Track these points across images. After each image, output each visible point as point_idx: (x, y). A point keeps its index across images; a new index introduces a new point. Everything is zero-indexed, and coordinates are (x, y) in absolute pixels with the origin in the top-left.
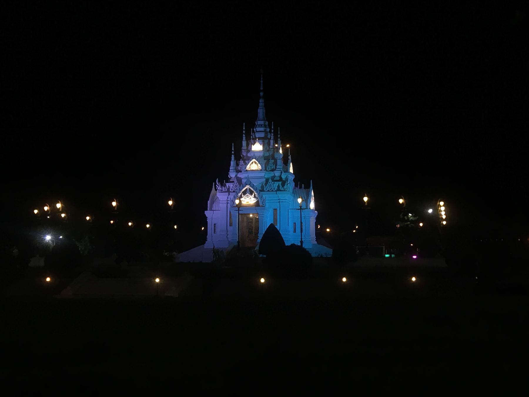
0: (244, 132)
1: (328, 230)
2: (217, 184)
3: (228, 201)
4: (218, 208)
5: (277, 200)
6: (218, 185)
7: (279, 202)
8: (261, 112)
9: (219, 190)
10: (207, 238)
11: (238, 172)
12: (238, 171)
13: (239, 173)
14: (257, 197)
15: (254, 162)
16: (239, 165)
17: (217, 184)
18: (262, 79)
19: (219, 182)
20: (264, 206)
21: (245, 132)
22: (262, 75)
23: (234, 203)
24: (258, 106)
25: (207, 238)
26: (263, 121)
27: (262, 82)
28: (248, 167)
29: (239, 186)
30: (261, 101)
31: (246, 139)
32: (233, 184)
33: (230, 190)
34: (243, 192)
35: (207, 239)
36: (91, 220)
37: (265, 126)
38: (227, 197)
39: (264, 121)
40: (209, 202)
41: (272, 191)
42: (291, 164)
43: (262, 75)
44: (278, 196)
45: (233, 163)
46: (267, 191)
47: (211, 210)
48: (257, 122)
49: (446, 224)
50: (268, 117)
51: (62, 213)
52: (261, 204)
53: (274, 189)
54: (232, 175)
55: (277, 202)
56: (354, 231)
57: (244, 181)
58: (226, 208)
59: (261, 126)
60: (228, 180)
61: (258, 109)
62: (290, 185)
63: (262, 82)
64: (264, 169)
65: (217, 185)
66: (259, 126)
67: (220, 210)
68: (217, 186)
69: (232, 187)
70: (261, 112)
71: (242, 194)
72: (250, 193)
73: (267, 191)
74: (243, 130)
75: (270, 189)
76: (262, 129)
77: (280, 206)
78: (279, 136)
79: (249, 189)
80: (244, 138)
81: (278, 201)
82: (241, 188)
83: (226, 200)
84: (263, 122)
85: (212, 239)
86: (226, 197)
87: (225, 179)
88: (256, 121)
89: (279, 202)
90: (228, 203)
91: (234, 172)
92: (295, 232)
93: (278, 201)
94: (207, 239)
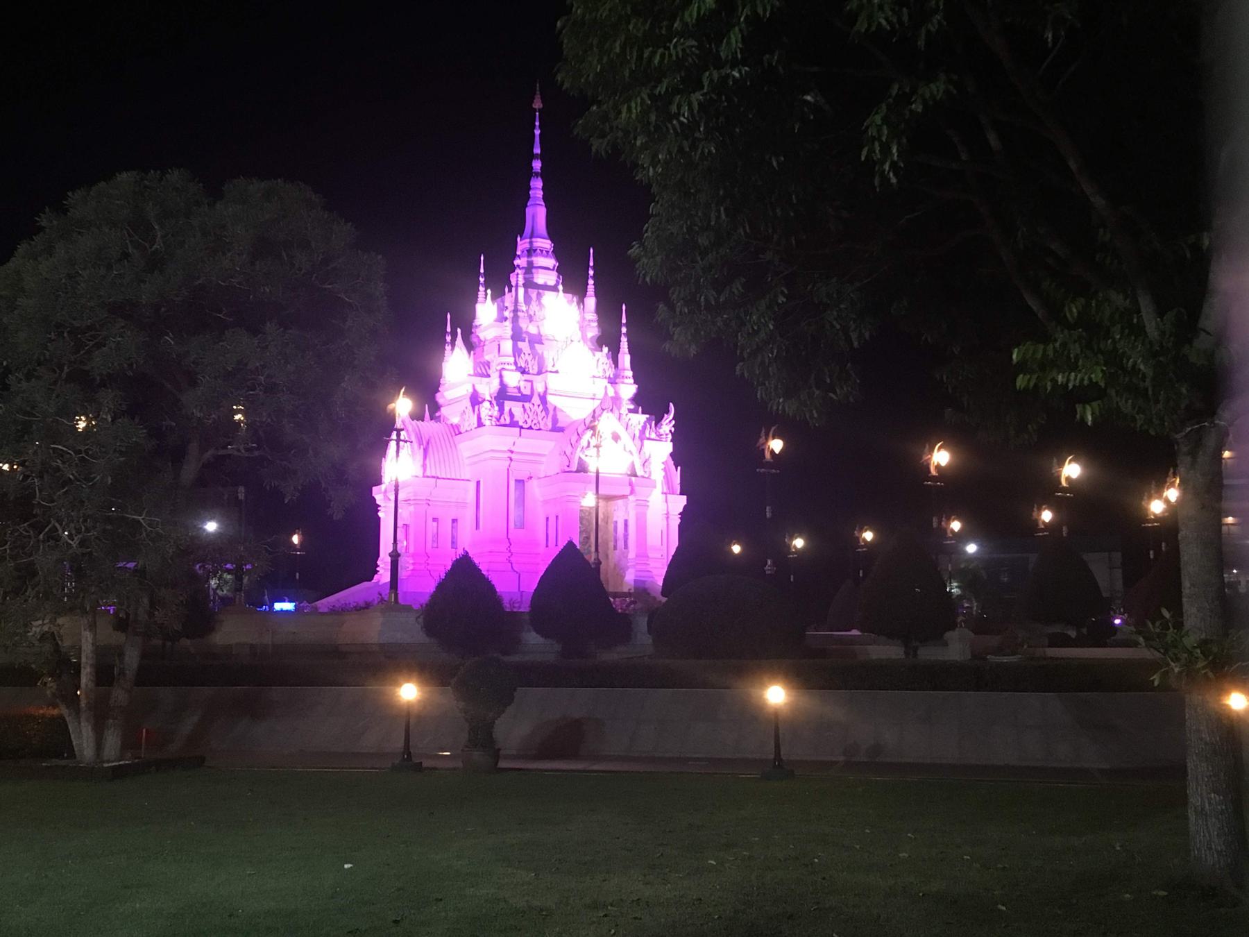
1: (736, 549)
7: (511, 459)
8: (538, 214)
10: (378, 566)
18: (537, 124)
20: (646, 476)
21: (485, 281)
22: (537, 114)
25: (378, 566)
27: (537, 132)
30: (537, 184)
31: (492, 295)
35: (378, 569)
43: (537, 114)
46: (528, 428)
49: (782, 451)
52: (640, 472)
56: (1072, 470)
61: (526, 206)
62: (627, 405)
63: (537, 132)
70: (538, 214)
73: (528, 428)
74: (620, 324)
78: (591, 273)
82: (573, 441)
85: (428, 564)
94: (378, 569)
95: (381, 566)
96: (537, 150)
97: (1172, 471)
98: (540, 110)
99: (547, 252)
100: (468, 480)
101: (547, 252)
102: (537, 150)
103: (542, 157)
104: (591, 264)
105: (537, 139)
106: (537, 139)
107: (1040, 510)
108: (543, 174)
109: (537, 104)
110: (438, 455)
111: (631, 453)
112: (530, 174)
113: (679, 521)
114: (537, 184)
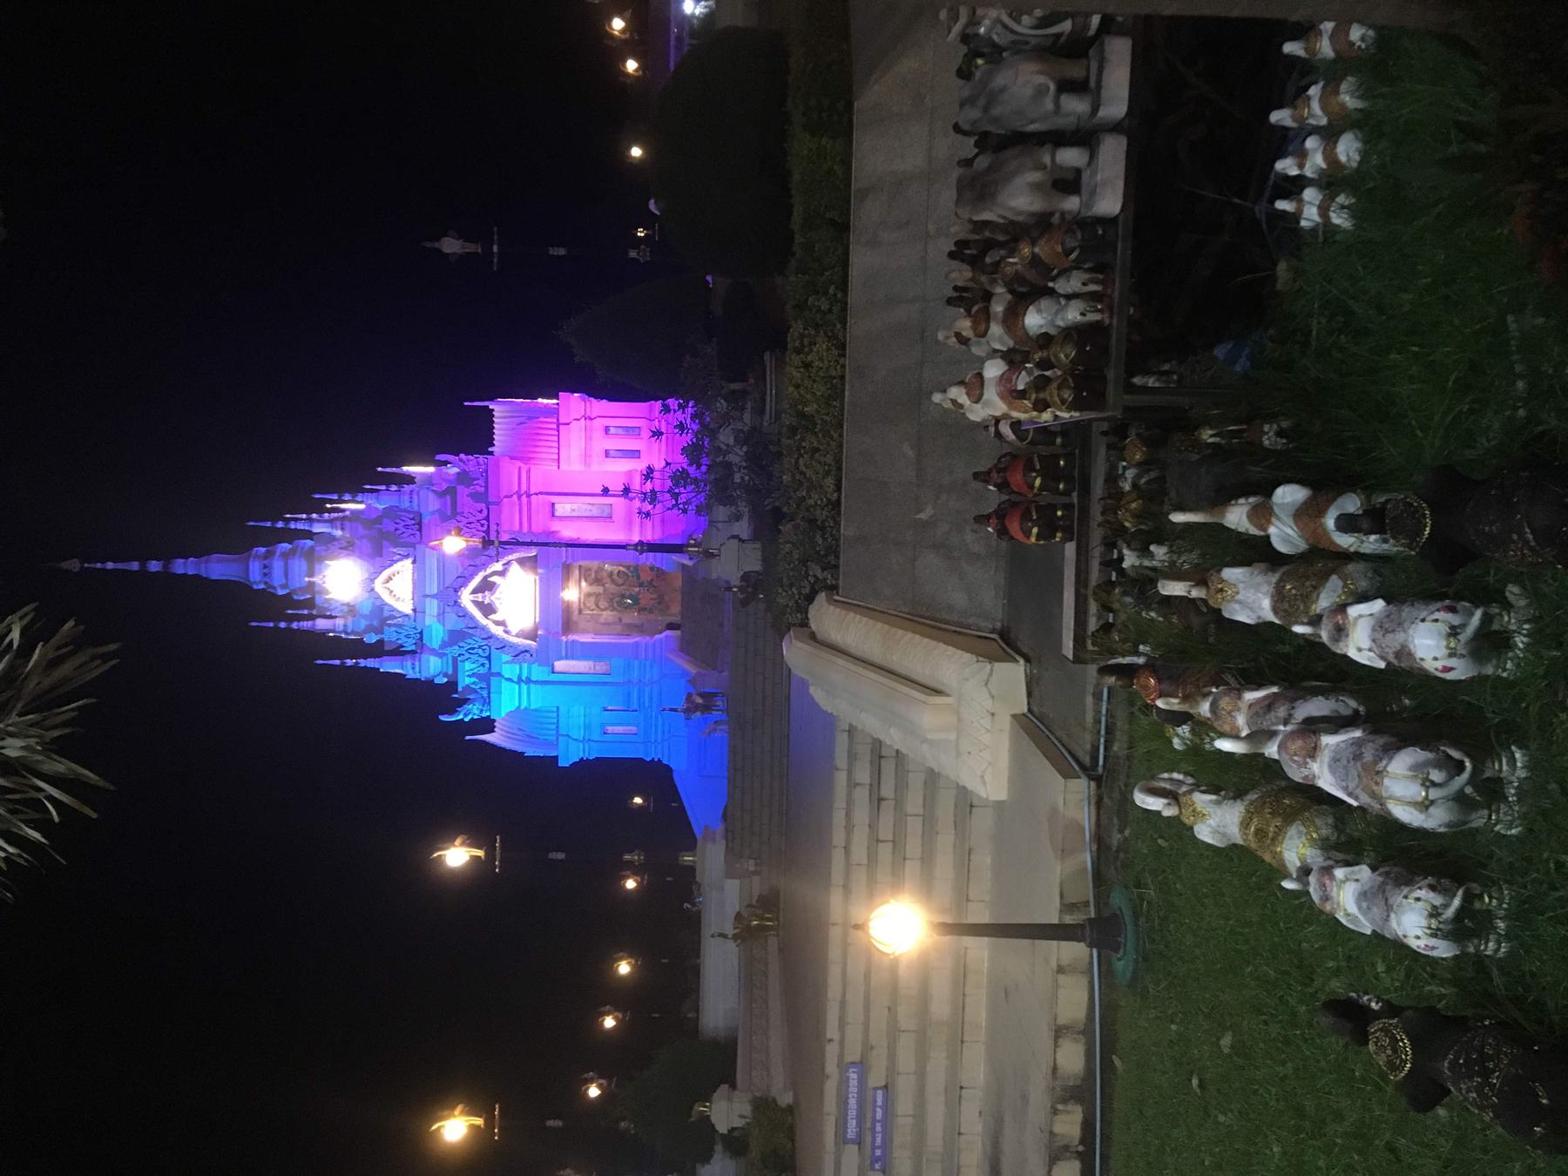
0: (154, 566)
2: (462, 720)
3: (520, 680)
4: (550, 715)
5: (520, 505)
6: (466, 715)
8: (218, 568)
9: (482, 710)
10: (653, 759)
11: (423, 646)
12: (420, 648)
13: (424, 642)
14: (504, 565)
15: (387, 585)
16: (399, 642)
17: (461, 717)
19: (453, 712)
23: (527, 651)
24: (197, 577)
25: (653, 759)
26: (251, 563)
27: (110, 565)
28: (406, 607)
29: (469, 641)
30: (180, 567)
32: (463, 661)
33: (483, 670)
34: (486, 616)
35: (656, 760)
36: (616, 1014)
37: (268, 555)
38: (508, 683)
39: (252, 559)
40: (530, 752)
41: (487, 518)
42: (405, 468)
44: (506, 497)
45: (390, 666)
47: (556, 745)
48: (255, 583)
50: (241, 544)
51: (616, 1006)
53: (481, 512)
54: (432, 667)
55: (529, 503)
57: (453, 622)
58: (549, 687)
59: (267, 571)
60: (452, 685)
63: (110, 565)
64: (412, 549)
65: (467, 720)
66: (265, 575)
67: (558, 708)
68: (470, 717)
69: (474, 663)
70: (218, 568)
71: (491, 617)
72: (490, 590)
75: (482, 525)
76: (278, 565)
77: (541, 493)
79: (475, 592)
80: (306, 625)
81: (524, 498)
83: (517, 686)
84: (253, 561)
86: (505, 684)
87: (446, 695)
88: (252, 588)
89: (529, 496)
90: (529, 681)
91: (420, 660)
92: (639, 451)
93: (524, 498)
94: (656, 760)
95: (653, 756)
96: (135, 566)
97: (1193, 584)
98: (82, 563)
99: (265, 567)
100: (559, 467)
101: (265, 567)
102: (135, 566)
103: (144, 560)
104: (269, 524)
105: (120, 566)
106: (120, 566)
107: (633, 967)
108: (168, 558)
109: (74, 565)
110: (542, 434)
111: (508, 563)
112: (167, 576)
113: (604, 401)
114: (180, 567)
